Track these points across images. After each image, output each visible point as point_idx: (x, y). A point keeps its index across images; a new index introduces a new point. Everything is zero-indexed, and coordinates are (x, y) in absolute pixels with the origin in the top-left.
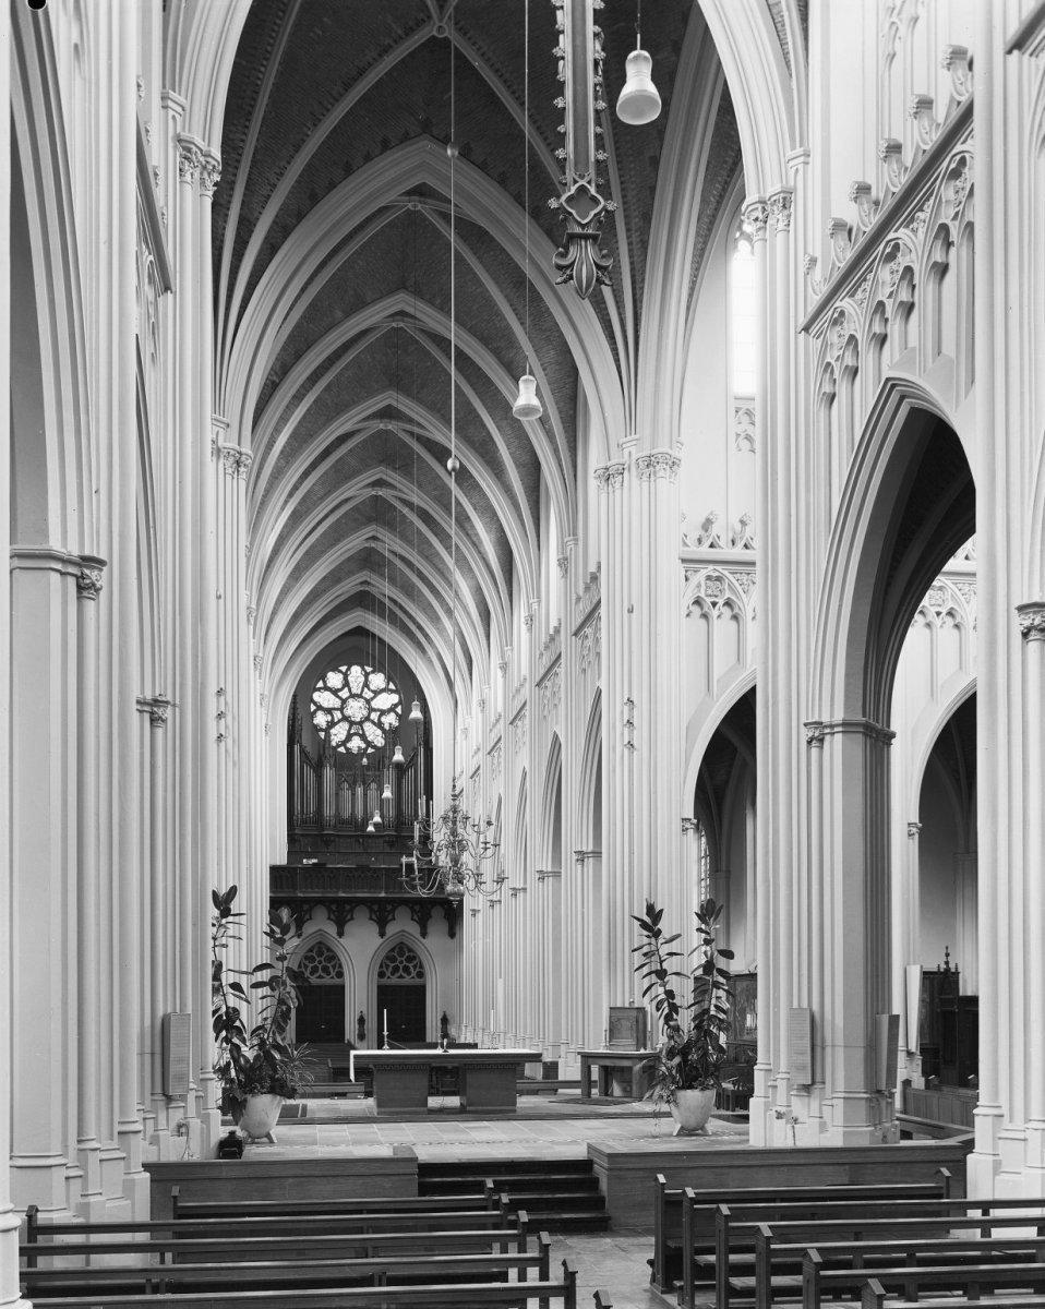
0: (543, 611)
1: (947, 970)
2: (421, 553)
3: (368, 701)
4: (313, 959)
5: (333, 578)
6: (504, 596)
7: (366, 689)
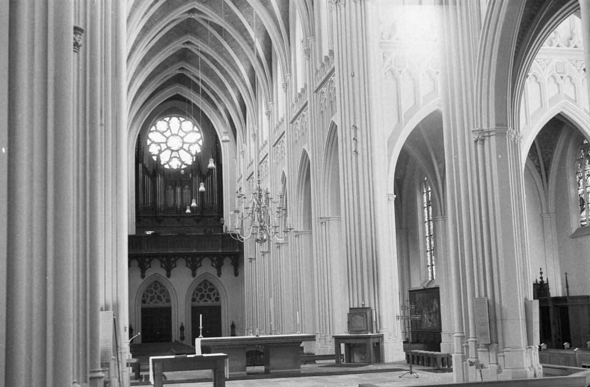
0: (248, 148)
1: (542, 282)
2: (217, 50)
3: (182, 138)
4: (151, 292)
5: (163, 66)
6: (243, 121)
7: (180, 131)
